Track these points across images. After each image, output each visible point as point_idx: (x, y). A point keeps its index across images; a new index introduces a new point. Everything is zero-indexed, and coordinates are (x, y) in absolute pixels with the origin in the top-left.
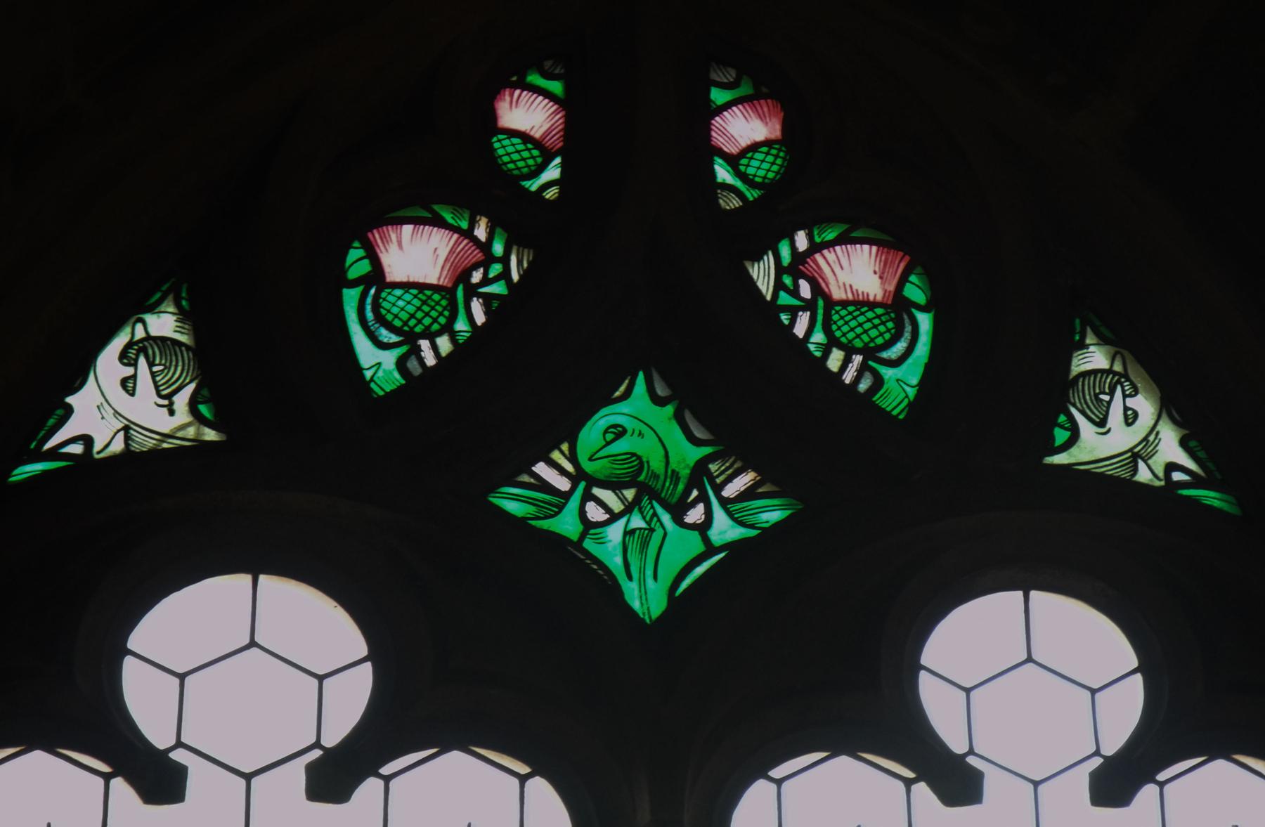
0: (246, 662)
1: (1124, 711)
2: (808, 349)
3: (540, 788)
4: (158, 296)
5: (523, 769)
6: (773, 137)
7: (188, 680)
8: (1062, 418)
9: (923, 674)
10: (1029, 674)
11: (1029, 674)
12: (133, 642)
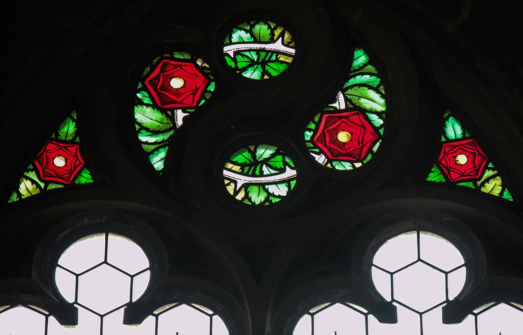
0: (103, 268)
1: (458, 282)
2: (267, 142)
3: (217, 319)
4: (55, 143)
5: (211, 312)
6: (70, 118)
7: (421, 258)
8: (226, 182)
9: (373, 267)
10: (419, 266)
11: (419, 266)
12: (60, 262)
